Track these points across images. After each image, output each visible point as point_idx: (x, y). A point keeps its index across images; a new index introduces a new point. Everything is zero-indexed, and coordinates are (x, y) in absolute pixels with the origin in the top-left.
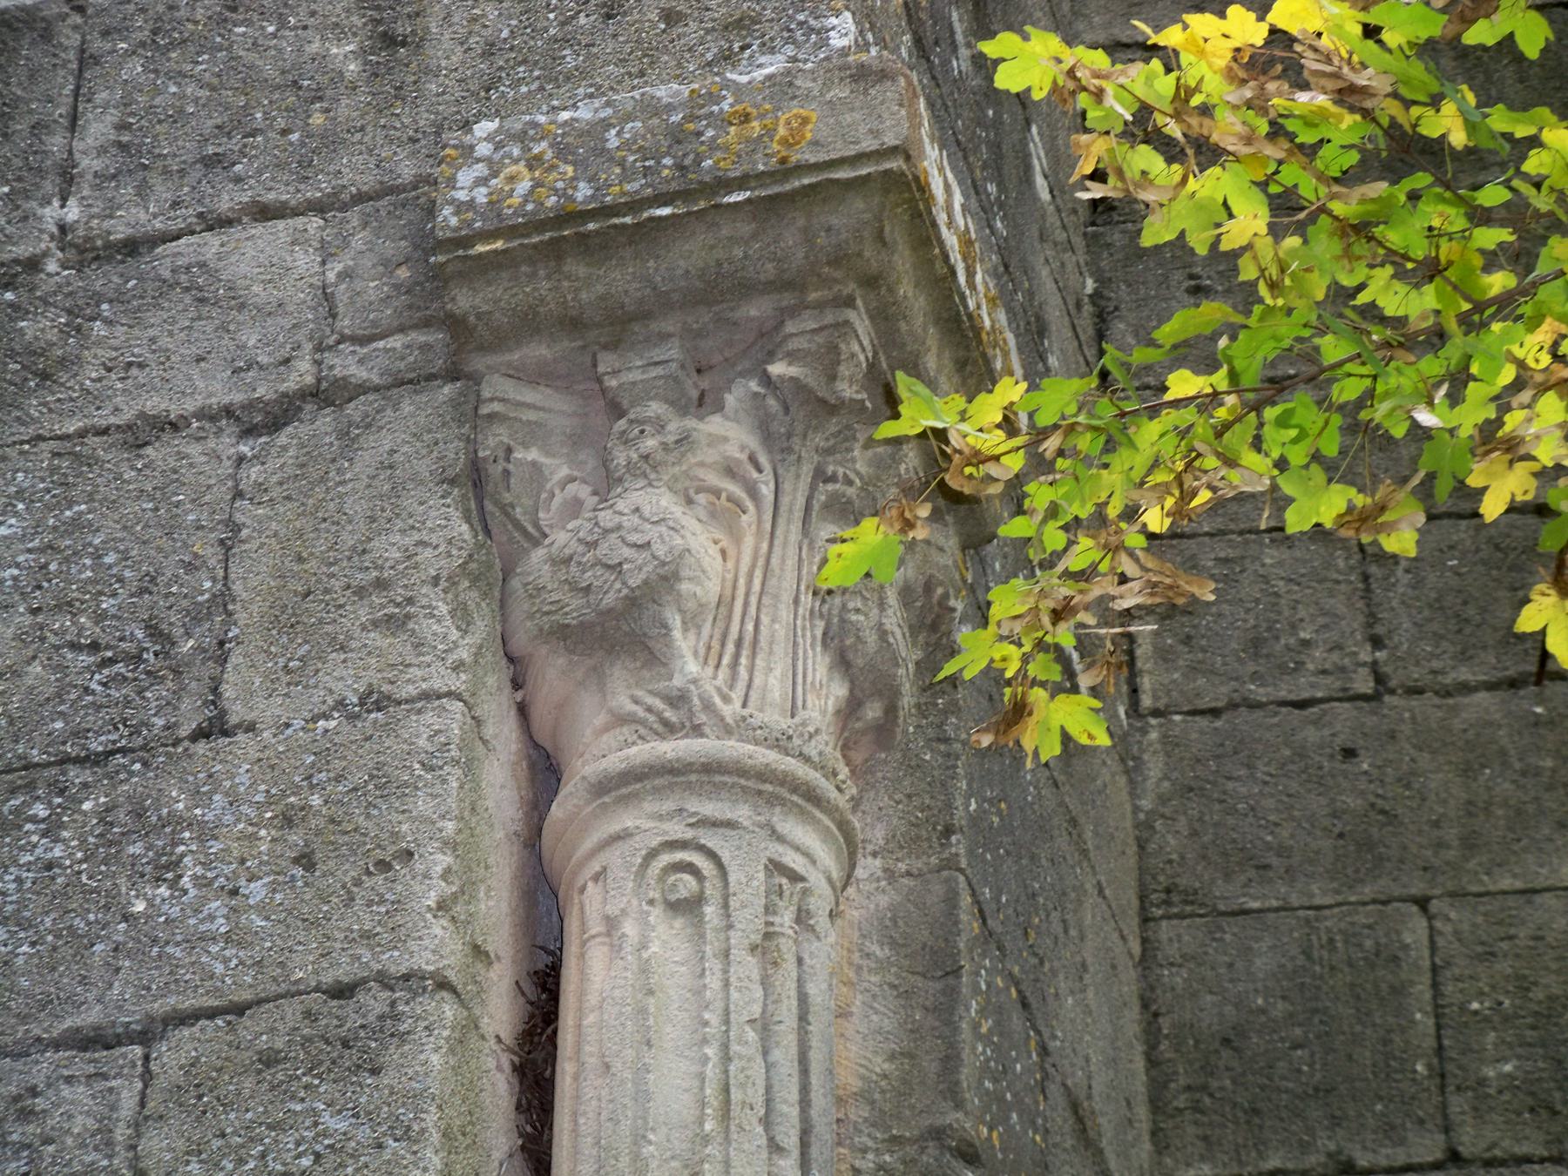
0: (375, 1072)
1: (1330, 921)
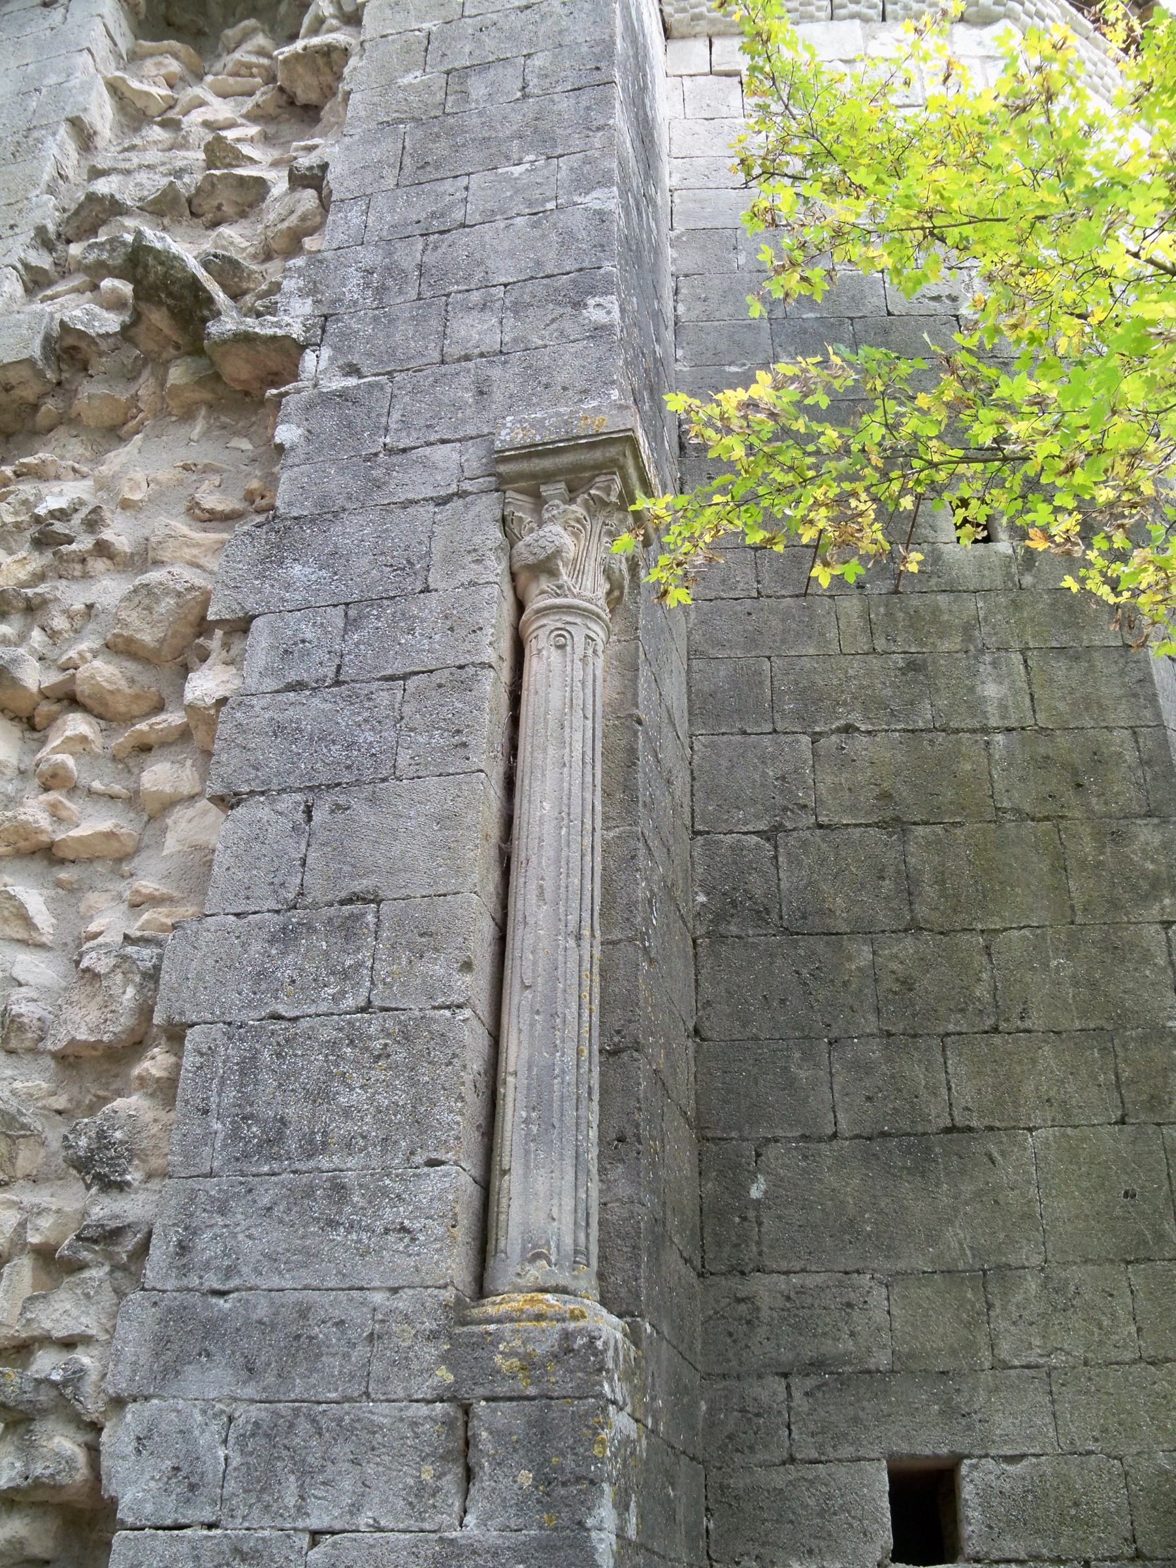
1: (742, 662)
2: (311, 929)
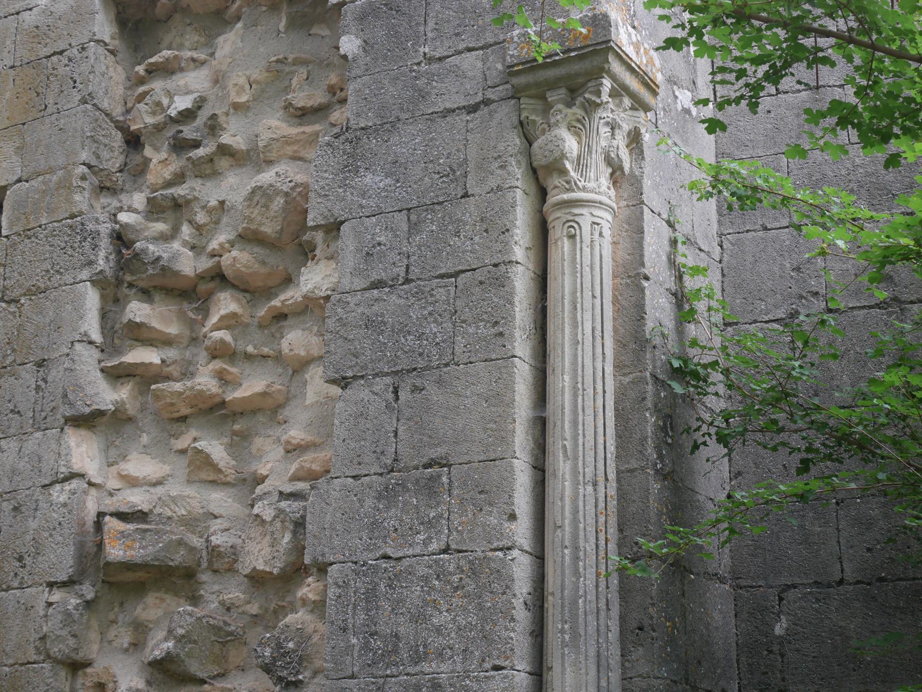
0: (503, 287)
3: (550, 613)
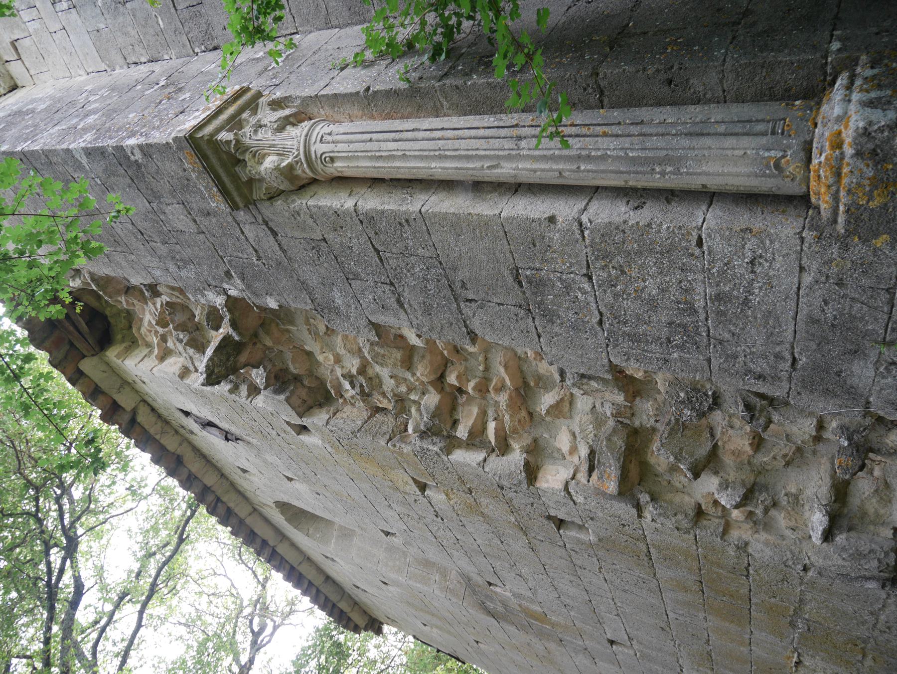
2: (541, 303)
3: (646, 184)
